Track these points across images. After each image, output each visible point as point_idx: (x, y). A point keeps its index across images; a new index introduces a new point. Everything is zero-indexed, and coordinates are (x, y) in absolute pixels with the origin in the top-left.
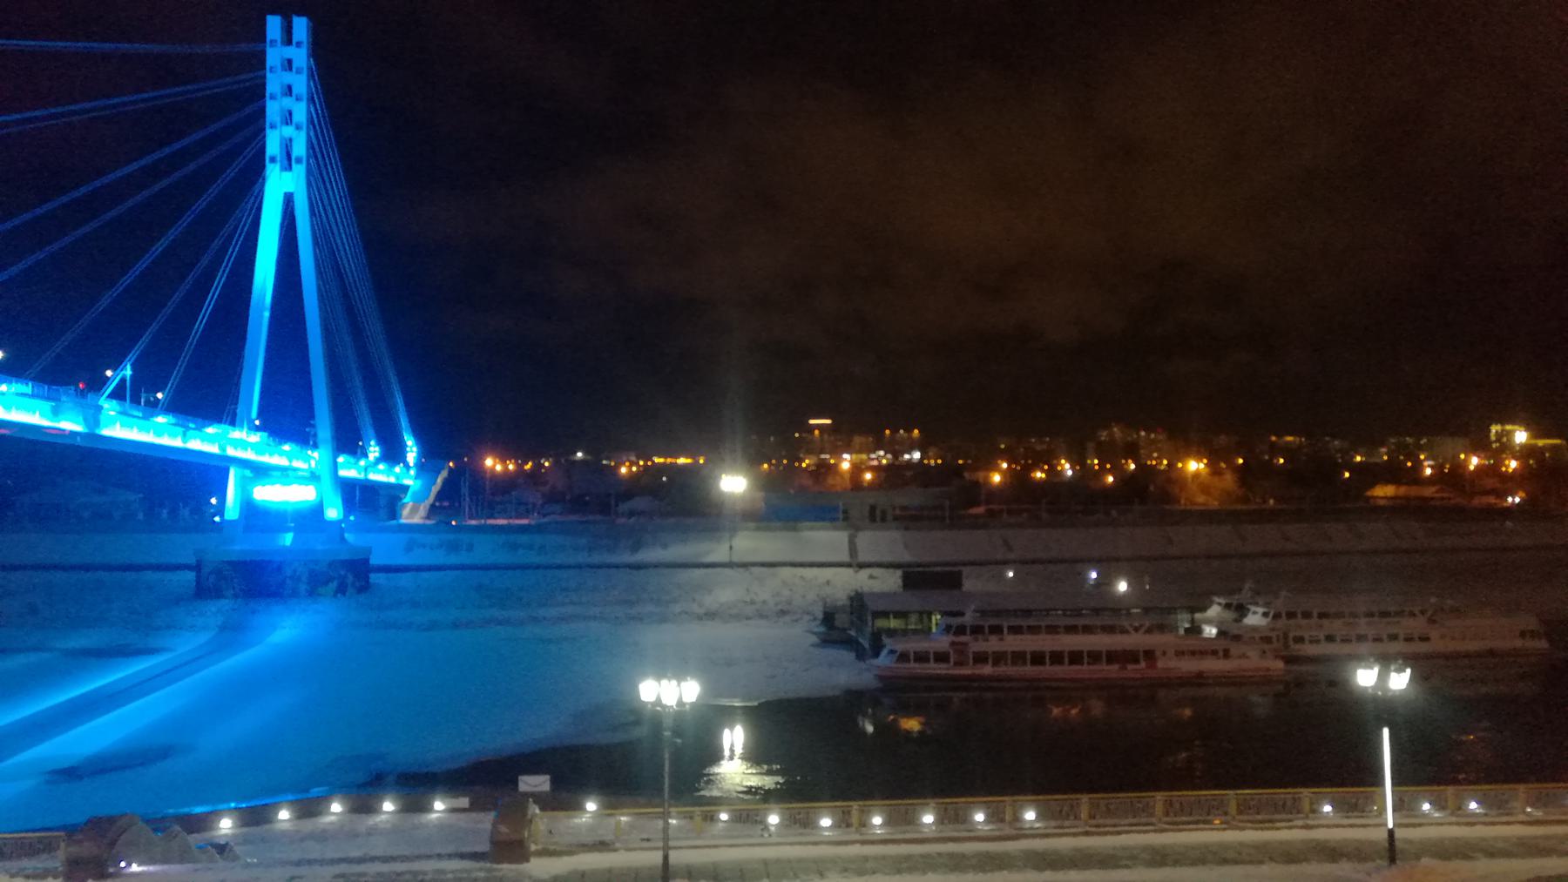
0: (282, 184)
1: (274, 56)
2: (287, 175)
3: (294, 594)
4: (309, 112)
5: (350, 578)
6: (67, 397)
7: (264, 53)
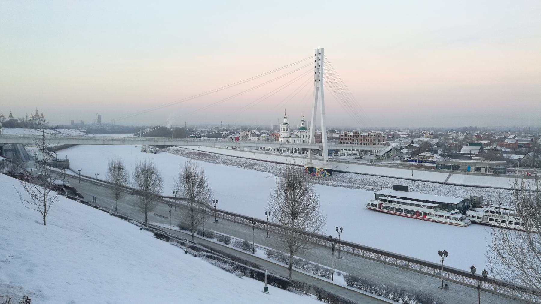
5: (327, 173)
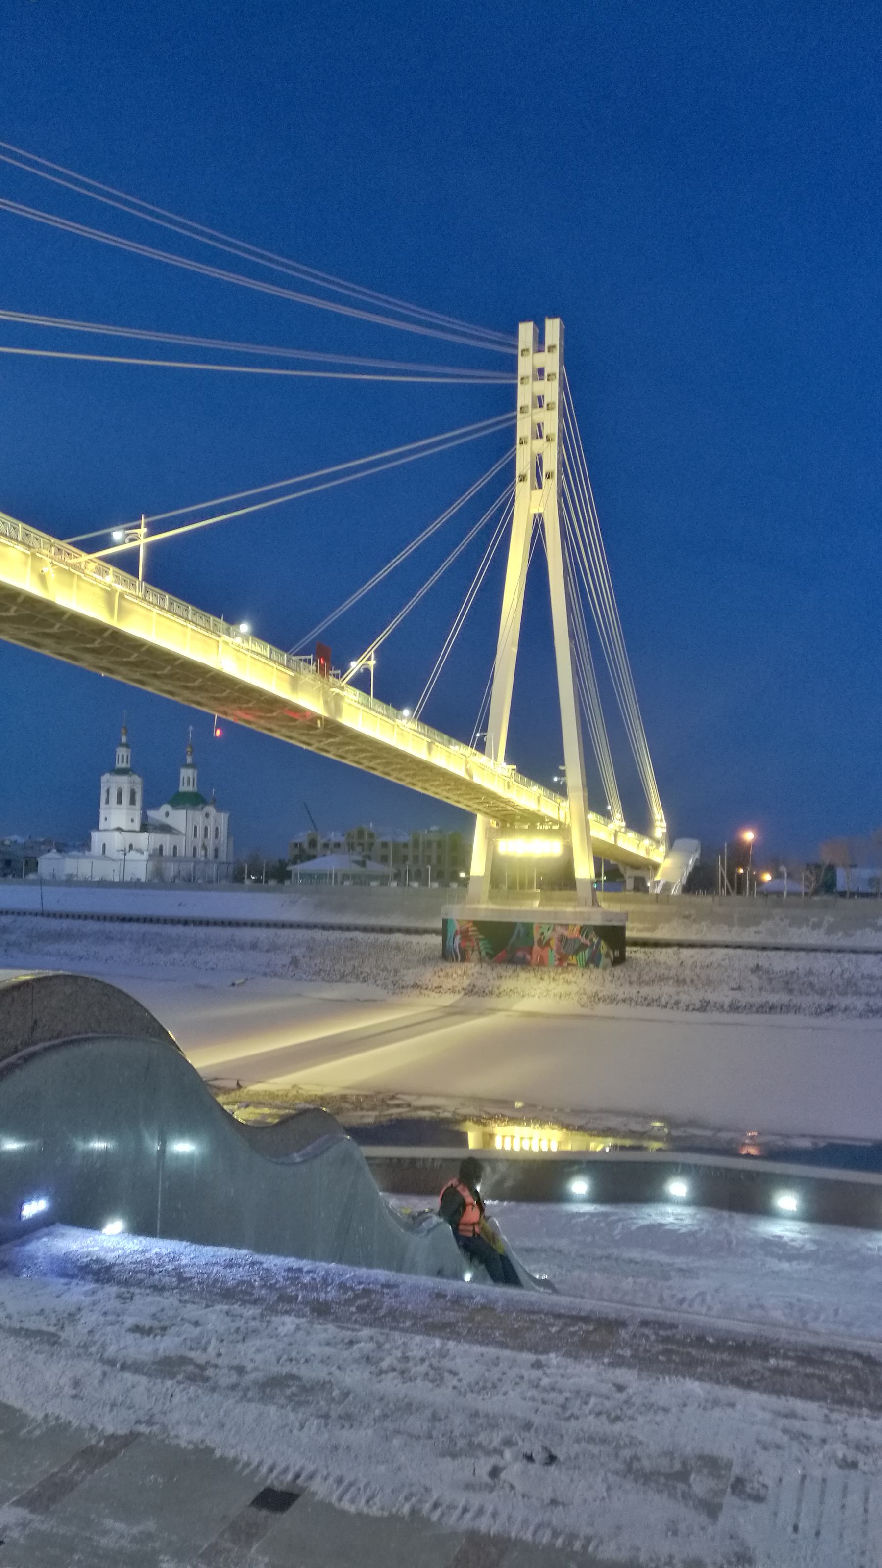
0: (534, 503)
1: (525, 366)
2: (538, 493)
3: (542, 963)
4: (560, 452)
5: (604, 948)
6: (309, 675)
7: (514, 387)
